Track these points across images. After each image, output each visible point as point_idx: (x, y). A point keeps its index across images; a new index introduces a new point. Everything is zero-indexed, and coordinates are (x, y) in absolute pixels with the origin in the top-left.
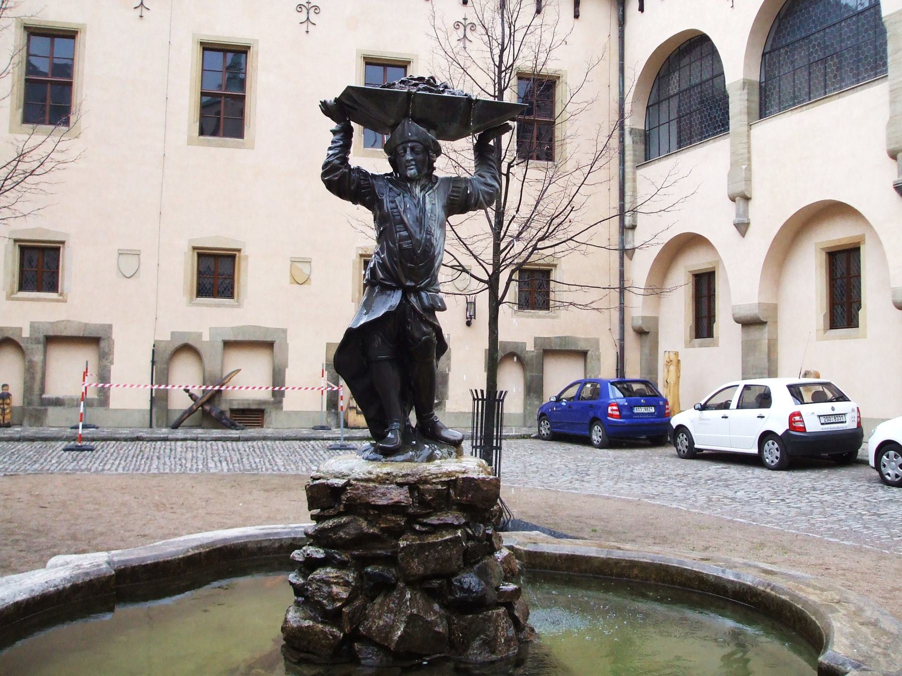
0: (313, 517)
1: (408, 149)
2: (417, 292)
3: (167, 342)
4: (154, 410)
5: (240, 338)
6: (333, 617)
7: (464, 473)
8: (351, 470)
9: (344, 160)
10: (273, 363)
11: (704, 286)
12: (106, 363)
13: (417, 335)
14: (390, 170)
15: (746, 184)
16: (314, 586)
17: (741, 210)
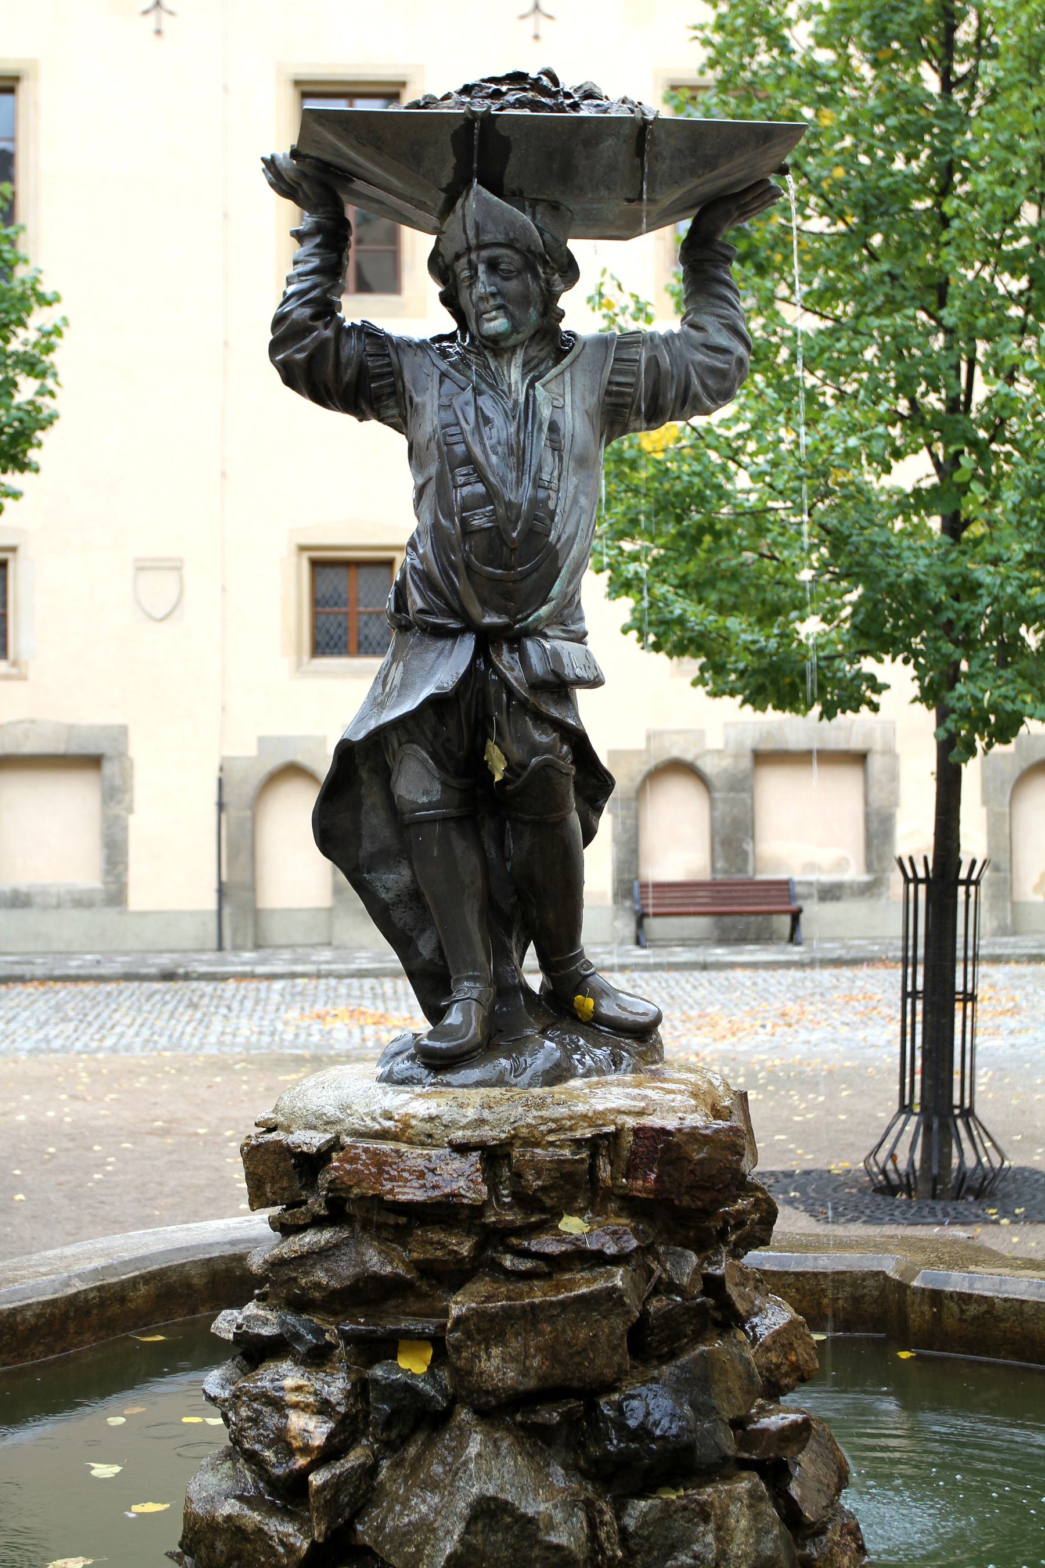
1: (481, 268)
2: (515, 638)
3: (248, 758)
4: (227, 911)
7: (641, 1113)
8: (345, 1107)
9: (326, 310)
12: (117, 810)
14: (450, 325)
16: (244, 1412)
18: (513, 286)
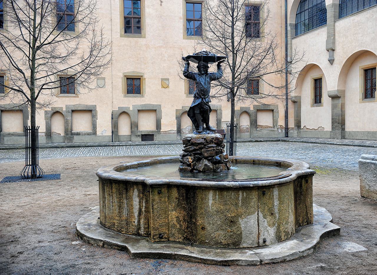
0: (184, 147)
4: (113, 136)
5: (144, 109)
6: (189, 165)
9: (188, 70)
10: (157, 118)
11: (318, 83)
13: (205, 108)
15: (333, 45)
17: (331, 54)
18: (204, 70)
